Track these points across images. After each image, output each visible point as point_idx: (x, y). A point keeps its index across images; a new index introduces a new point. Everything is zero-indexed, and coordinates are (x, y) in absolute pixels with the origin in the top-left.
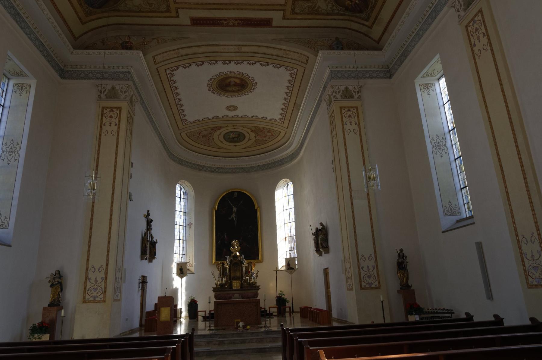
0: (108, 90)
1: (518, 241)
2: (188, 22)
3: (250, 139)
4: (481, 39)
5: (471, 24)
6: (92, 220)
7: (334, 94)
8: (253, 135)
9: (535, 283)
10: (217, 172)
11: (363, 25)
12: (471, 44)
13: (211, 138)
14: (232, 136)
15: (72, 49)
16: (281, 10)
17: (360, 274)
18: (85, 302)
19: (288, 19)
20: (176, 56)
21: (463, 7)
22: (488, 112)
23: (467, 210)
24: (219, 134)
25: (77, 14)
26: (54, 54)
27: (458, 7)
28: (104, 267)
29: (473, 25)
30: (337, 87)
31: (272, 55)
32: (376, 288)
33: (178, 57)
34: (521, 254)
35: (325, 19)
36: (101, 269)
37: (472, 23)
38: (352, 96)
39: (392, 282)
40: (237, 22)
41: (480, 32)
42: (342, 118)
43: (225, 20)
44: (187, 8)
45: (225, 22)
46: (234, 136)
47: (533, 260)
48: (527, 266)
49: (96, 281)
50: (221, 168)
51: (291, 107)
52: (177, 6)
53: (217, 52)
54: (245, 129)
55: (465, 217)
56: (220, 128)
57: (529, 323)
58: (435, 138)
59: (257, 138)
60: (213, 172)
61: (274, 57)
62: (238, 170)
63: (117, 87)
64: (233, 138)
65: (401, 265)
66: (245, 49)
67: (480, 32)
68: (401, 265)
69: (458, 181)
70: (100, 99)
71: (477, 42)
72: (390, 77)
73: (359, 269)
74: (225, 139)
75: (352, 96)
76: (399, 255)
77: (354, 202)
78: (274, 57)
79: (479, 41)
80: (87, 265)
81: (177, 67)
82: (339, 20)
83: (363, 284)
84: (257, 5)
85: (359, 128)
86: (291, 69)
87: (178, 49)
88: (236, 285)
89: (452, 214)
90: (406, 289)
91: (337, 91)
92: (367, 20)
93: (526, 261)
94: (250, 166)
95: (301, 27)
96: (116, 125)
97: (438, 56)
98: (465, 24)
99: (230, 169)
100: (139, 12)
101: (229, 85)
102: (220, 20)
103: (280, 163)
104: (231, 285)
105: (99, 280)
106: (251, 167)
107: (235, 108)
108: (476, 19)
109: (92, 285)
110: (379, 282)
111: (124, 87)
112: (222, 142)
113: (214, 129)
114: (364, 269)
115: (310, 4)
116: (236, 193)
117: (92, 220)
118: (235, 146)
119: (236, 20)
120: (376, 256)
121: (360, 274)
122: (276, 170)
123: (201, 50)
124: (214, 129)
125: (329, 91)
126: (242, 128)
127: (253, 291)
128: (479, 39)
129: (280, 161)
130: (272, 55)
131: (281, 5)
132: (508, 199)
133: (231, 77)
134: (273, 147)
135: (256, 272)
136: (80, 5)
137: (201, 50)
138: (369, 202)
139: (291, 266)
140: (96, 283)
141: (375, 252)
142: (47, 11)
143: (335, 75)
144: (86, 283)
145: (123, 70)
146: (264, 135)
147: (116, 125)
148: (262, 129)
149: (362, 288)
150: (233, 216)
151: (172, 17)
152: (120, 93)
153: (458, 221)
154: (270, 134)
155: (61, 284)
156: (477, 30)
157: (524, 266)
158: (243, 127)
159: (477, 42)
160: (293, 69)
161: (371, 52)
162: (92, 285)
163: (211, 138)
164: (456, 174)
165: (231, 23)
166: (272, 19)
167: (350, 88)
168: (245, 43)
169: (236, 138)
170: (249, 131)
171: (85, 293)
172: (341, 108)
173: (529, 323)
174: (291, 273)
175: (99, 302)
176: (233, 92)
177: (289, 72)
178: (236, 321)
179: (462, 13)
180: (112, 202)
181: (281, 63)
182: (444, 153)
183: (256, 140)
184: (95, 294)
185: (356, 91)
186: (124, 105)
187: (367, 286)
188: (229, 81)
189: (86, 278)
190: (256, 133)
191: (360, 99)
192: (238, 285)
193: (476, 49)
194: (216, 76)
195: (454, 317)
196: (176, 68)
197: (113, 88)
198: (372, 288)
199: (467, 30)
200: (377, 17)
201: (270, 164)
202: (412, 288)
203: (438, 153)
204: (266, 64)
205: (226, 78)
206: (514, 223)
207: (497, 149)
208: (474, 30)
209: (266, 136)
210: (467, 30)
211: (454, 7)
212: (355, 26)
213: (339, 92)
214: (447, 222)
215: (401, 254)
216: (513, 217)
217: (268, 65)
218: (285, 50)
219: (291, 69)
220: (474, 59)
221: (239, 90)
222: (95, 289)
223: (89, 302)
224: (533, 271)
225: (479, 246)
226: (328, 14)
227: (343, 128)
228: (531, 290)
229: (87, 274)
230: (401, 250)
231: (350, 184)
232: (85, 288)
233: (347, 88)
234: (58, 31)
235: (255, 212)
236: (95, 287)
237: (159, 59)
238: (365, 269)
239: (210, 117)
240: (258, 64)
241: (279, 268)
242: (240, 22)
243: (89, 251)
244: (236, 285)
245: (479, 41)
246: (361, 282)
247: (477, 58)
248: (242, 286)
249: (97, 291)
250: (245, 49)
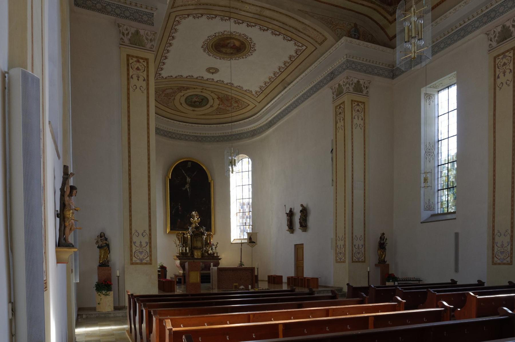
0: (132, 33)
1: (493, 234)
3: (212, 106)
4: (507, 73)
5: (500, 57)
6: (130, 184)
7: (348, 86)
8: (217, 102)
9: (499, 262)
10: (170, 137)
11: (385, 17)
12: (495, 75)
13: (173, 98)
14: (195, 99)
17: (353, 250)
18: (132, 264)
21: (496, 38)
22: (494, 137)
23: (439, 207)
24: (182, 94)
27: (493, 37)
28: (148, 232)
29: (502, 58)
30: (351, 79)
31: (290, 26)
32: (362, 262)
34: (493, 243)
36: (144, 234)
37: (502, 56)
38: (361, 91)
39: (372, 257)
41: (508, 67)
42: (352, 111)
46: (196, 100)
47: (502, 247)
48: (496, 250)
49: (141, 245)
50: (174, 133)
51: (279, 81)
54: (213, 95)
55: (437, 213)
56: (188, 88)
57: (508, 284)
58: (428, 145)
59: (221, 106)
60: (165, 136)
61: (291, 29)
62: (191, 138)
63: (142, 32)
64: (195, 102)
65: (382, 246)
66: (267, 13)
67: (508, 67)
68: (382, 246)
69: (437, 184)
70: (122, 43)
71: (501, 75)
72: (393, 77)
73: (352, 247)
74: (186, 102)
75: (361, 91)
76: (381, 238)
77: (354, 191)
78: (291, 29)
79: (504, 76)
80: (131, 229)
83: (354, 258)
85: (364, 124)
86: (301, 45)
88: (197, 254)
89: (429, 209)
90: (382, 263)
91: (351, 83)
93: (496, 248)
94: (204, 135)
95: (329, 4)
96: (144, 80)
97: (455, 72)
98: (495, 55)
99: (183, 135)
101: (225, 46)
103: (238, 137)
104: (192, 254)
105: (144, 244)
106: (205, 137)
107: (216, 71)
108: (507, 54)
109: (137, 248)
110: (365, 257)
111: (149, 33)
112: (181, 104)
113: (181, 89)
114: (136, 244)
116: (190, 163)
117: (130, 184)
118: (193, 110)
120: (365, 237)
121: (353, 250)
122: (235, 143)
124: (181, 89)
125: (340, 79)
126: (209, 93)
127: (216, 261)
128: (504, 73)
129: (238, 134)
130: (290, 26)
132: (494, 205)
133: (233, 38)
134: (234, 119)
135: (215, 244)
138: (365, 193)
139: (253, 240)
140: (141, 247)
141: (365, 234)
143: (351, 65)
144: (131, 247)
145: (146, 10)
146: (229, 105)
147: (144, 80)
148: (230, 98)
149: (353, 262)
150: (187, 186)
152: (146, 41)
153: (433, 215)
154: (236, 105)
155: (108, 246)
156: (505, 64)
157: (493, 250)
158: (212, 92)
159: (501, 75)
160: (303, 45)
161: (381, 48)
162: (137, 248)
163: (173, 98)
164: (437, 177)
167: (362, 82)
168: (267, 6)
169: (197, 102)
170: (216, 97)
171: (131, 256)
172: (352, 101)
173: (508, 284)
174: (252, 247)
175: (146, 264)
176: (226, 53)
177: (296, 47)
178: (235, 284)
179: (494, 44)
180: (149, 168)
181: (294, 36)
182: (431, 159)
183: (218, 108)
184: (141, 257)
185: (366, 86)
186: (151, 56)
187: (357, 260)
188: (228, 42)
189: (131, 242)
190: (222, 100)
191: (367, 95)
192: (200, 254)
193: (499, 81)
195: (421, 283)
196: (186, 16)
197: (137, 32)
198: (359, 262)
199: (495, 62)
201: (222, 136)
202: (387, 263)
203: (428, 159)
204: (278, 33)
205: (231, 38)
206: (494, 222)
207: (494, 166)
208: (502, 64)
209: (231, 106)
210: (495, 62)
211: (488, 35)
212: (376, 16)
213: (352, 84)
214: (425, 215)
215: (383, 237)
216: (494, 217)
217: (278, 35)
218: (306, 24)
219: (301, 45)
220: (495, 89)
221: (232, 53)
222: (141, 253)
223: (137, 264)
224: (500, 254)
225: (457, 235)
227: (352, 122)
228: (495, 266)
229: (131, 238)
230: (383, 234)
231: (353, 175)
232: (131, 251)
233: (358, 82)
235: (210, 184)
236: (141, 250)
238: (356, 247)
239: (185, 76)
240: (270, 31)
241: (232, 240)
243: (130, 216)
244: (197, 254)
245: (504, 76)
246: (352, 257)
247: (497, 88)
248: (203, 256)
249: (143, 254)
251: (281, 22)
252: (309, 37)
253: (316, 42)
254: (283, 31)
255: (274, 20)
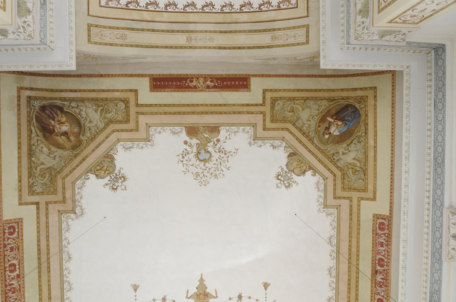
2: (254, 81)
11: (32, 89)
15: (405, 73)
16: (142, 105)
19: (131, 90)
20: (277, 33)
25: (375, 105)
26: (431, 80)
33: (274, 30)
35: (84, 91)
40: (194, 83)
43: (208, 87)
44: (252, 105)
45: (209, 83)
52: (262, 109)
53: (221, 32)
81: (279, 8)
82: (66, 91)
84: (170, 113)
87: (272, 47)
92: (29, 98)
100: (307, 98)
102: (214, 87)
115: (108, 115)
119: (195, 87)
123: (241, 39)
131: (143, 114)
136: (366, 115)
137: (241, 39)
142: (405, 140)
151: (271, 90)
165: (201, 80)
166: (151, 90)
194: (223, 148)
200: (19, 110)
226: (82, 100)
234: (407, 109)
237: (300, 35)
242: (191, 85)
250: (181, 39)
251: (158, 31)
252: (110, 28)
253: (96, 26)
254: (146, 16)
255: (168, 31)
